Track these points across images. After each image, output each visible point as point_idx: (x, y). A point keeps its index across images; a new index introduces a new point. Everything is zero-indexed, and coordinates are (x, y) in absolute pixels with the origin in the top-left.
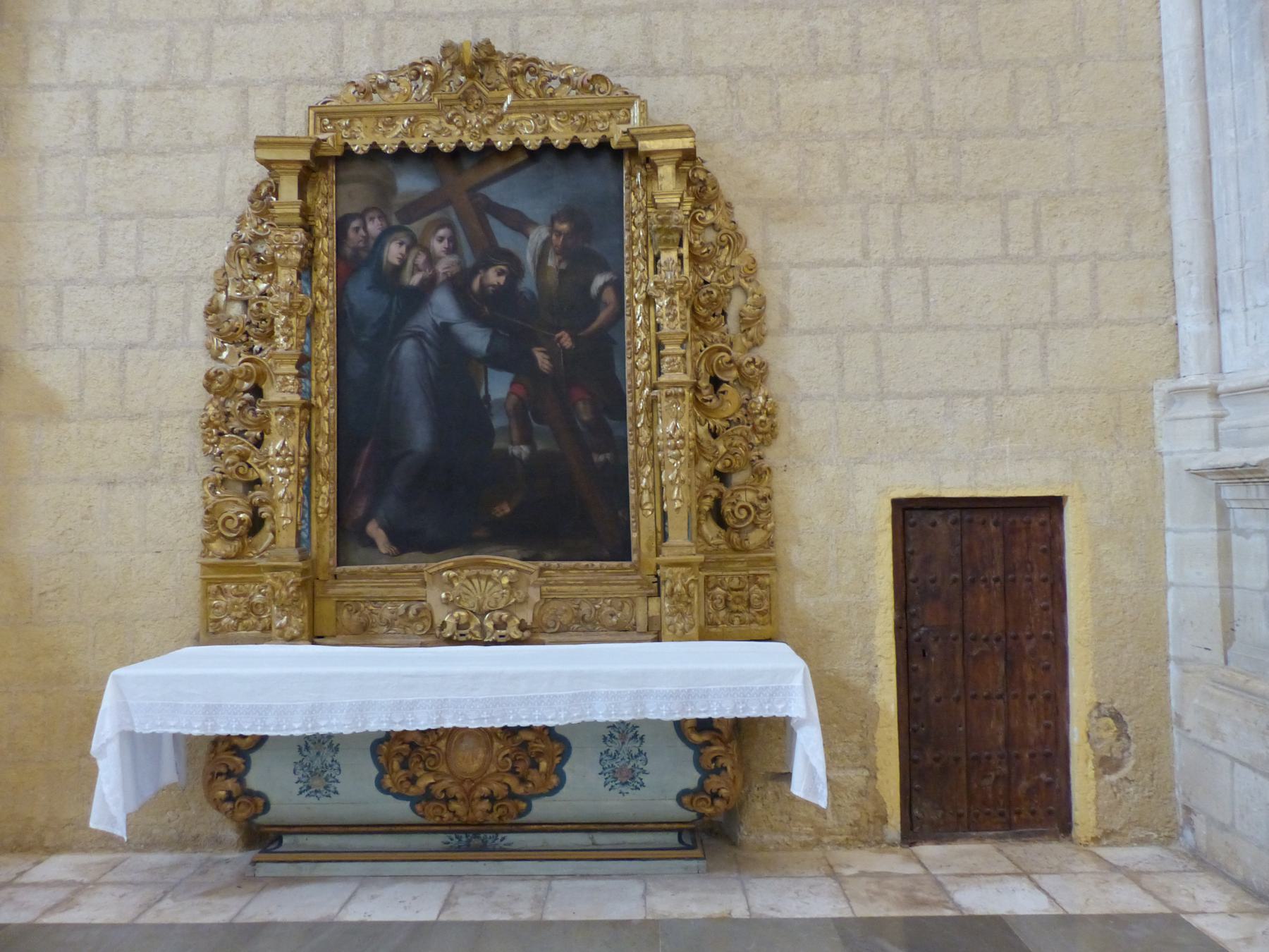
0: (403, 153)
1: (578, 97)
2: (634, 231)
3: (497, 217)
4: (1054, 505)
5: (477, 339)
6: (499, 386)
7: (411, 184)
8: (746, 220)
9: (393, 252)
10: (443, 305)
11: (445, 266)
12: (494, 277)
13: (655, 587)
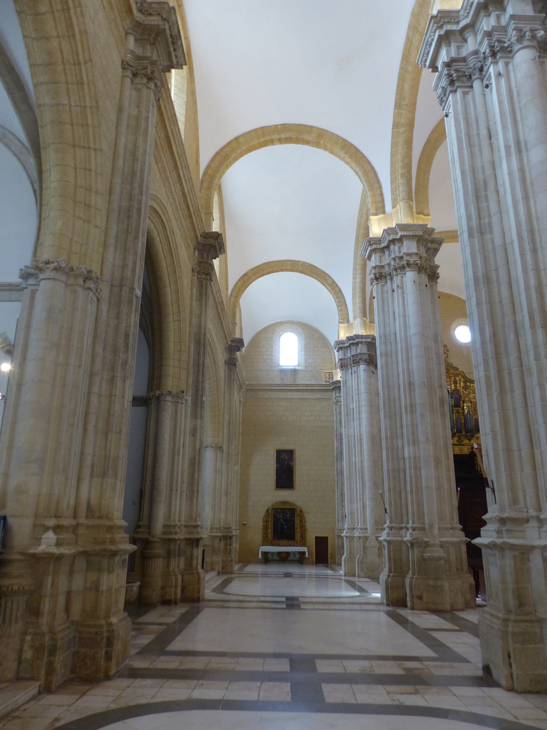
0: (279, 508)
1: (460, 241)
2: (296, 515)
3: (172, 639)
4: (327, 537)
5: (284, 523)
6: (285, 527)
7: (279, 510)
8: (304, 514)
9: (278, 515)
10: (281, 520)
11: (282, 517)
12: (285, 518)
13: (297, 543)
